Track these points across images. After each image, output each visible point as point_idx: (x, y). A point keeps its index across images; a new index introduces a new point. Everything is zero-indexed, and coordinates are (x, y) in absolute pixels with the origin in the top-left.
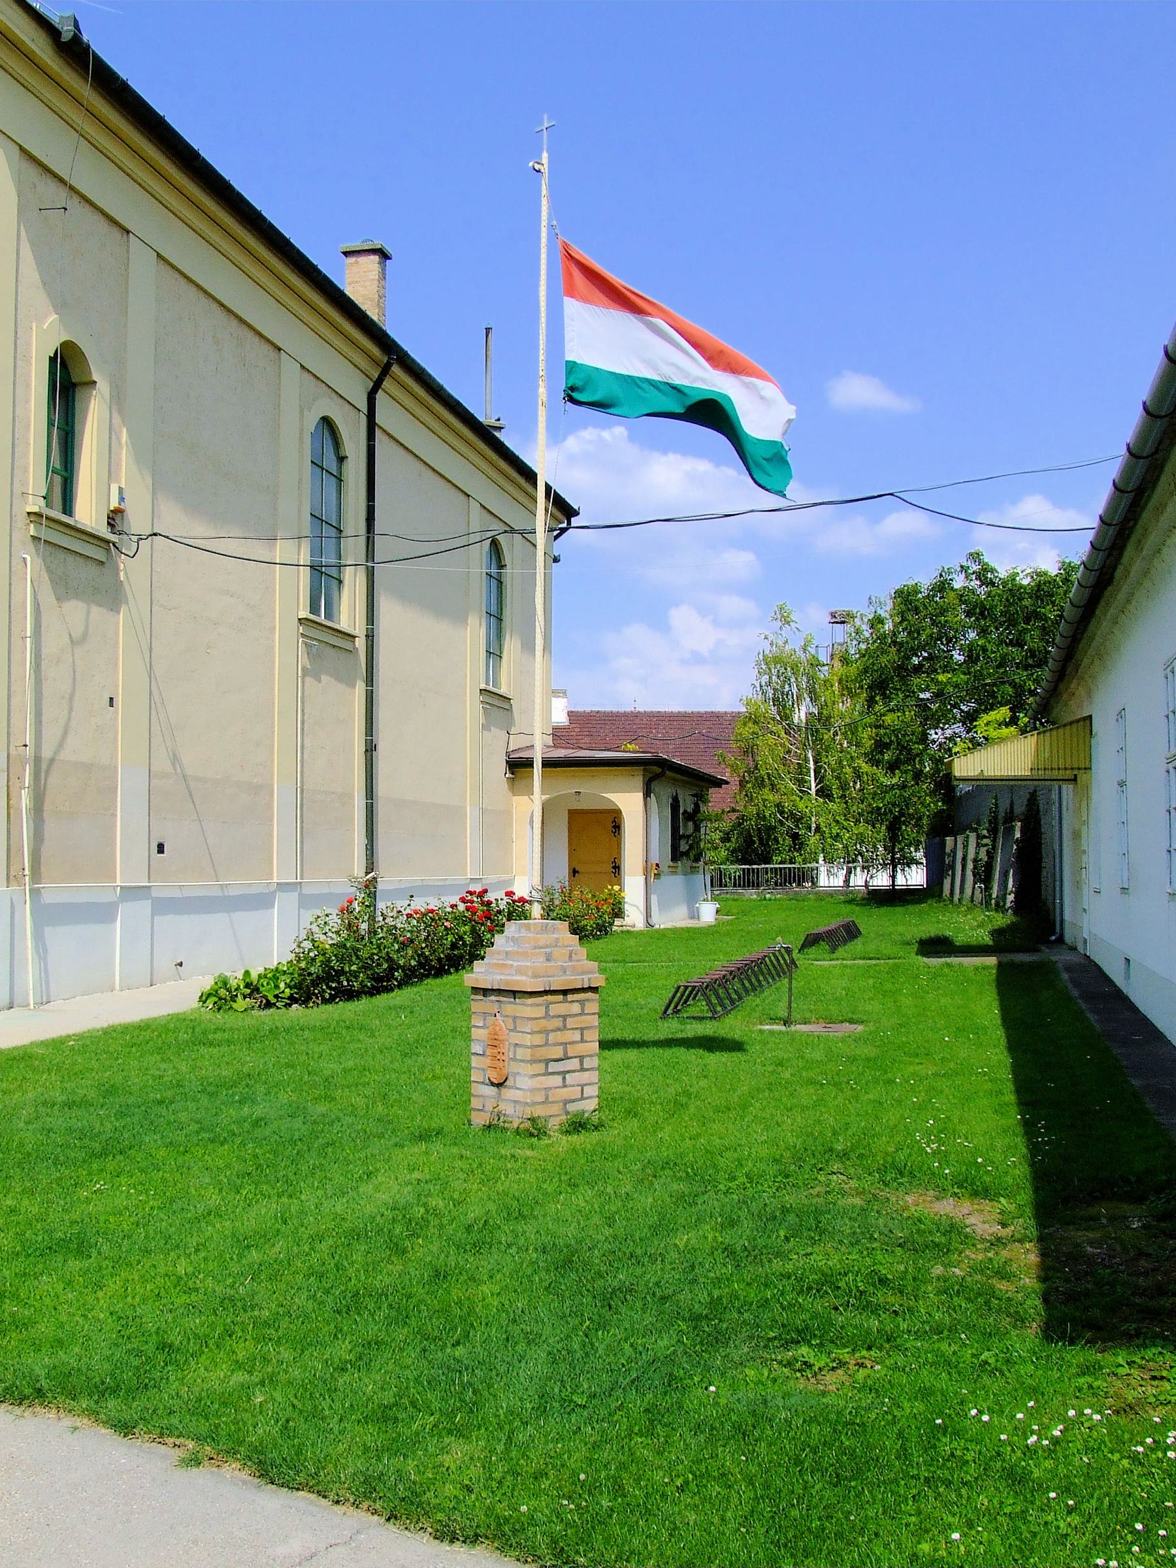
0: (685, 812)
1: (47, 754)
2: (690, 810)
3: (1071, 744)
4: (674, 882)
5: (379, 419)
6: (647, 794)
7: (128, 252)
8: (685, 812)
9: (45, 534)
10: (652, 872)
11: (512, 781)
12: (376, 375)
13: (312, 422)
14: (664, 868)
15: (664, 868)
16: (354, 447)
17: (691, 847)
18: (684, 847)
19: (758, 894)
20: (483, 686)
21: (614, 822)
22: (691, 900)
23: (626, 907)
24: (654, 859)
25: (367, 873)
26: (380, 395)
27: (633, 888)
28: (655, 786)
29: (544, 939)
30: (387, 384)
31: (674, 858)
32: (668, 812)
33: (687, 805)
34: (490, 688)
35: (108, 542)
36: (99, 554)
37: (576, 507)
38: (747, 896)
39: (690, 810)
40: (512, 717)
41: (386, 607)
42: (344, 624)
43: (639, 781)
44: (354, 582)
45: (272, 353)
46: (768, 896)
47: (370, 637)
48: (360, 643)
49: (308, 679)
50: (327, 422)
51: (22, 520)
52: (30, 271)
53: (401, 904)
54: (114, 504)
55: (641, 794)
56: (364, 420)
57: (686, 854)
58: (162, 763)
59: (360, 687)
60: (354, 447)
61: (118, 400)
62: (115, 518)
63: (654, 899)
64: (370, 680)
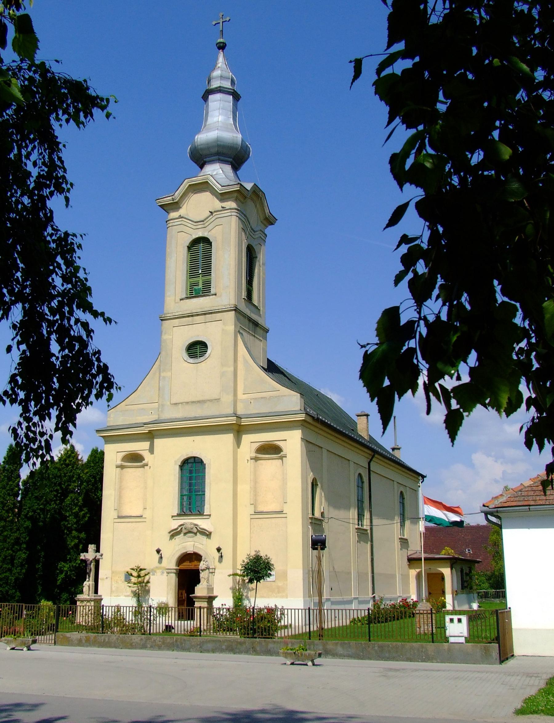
0: (466, 573)
1: (313, 569)
2: (467, 572)
3: (343, 631)
4: (463, 597)
5: (371, 469)
6: (452, 569)
7: (285, 396)
8: (466, 573)
9: (313, 522)
10: (455, 594)
11: (409, 565)
12: (370, 458)
13: (357, 475)
14: (459, 591)
15: (459, 591)
16: (366, 479)
17: (468, 584)
18: (466, 584)
19: (500, 601)
20: (400, 537)
21: (442, 577)
22: (470, 602)
23: (447, 604)
24: (455, 588)
25: (373, 594)
26: (372, 463)
27: (449, 598)
28: (454, 566)
29: (425, 605)
30: (374, 459)
31: (462, 589)
32: (460, 574)
33: (466, 570)
34: (402, 537)
35: (321, 520)
36: (319, 523)
37: (425, 475)
38: (495, 602)
39: (467, 572)
40: (408, 544)
41: (375, 522)
42: (365, 527)
43: (449, 565)
44: (367, 515)
45: (347, 462)
46: (503, 601)
47: (371, 529)
48: (369, 531)
49: (358, 543)
50: (360, 475)
51: (308, 518)
52: (308, 466)
53: (388, 602)
54: (322, 511)
55: (449, 569)
56: (367, 470)
57: (466, 587)
58: (332, 569)
59: (369, 543)
60: (366, 479)
61: (322, 488)
62: (322, 514)
63: (456, 602)
64: (372, 541)
